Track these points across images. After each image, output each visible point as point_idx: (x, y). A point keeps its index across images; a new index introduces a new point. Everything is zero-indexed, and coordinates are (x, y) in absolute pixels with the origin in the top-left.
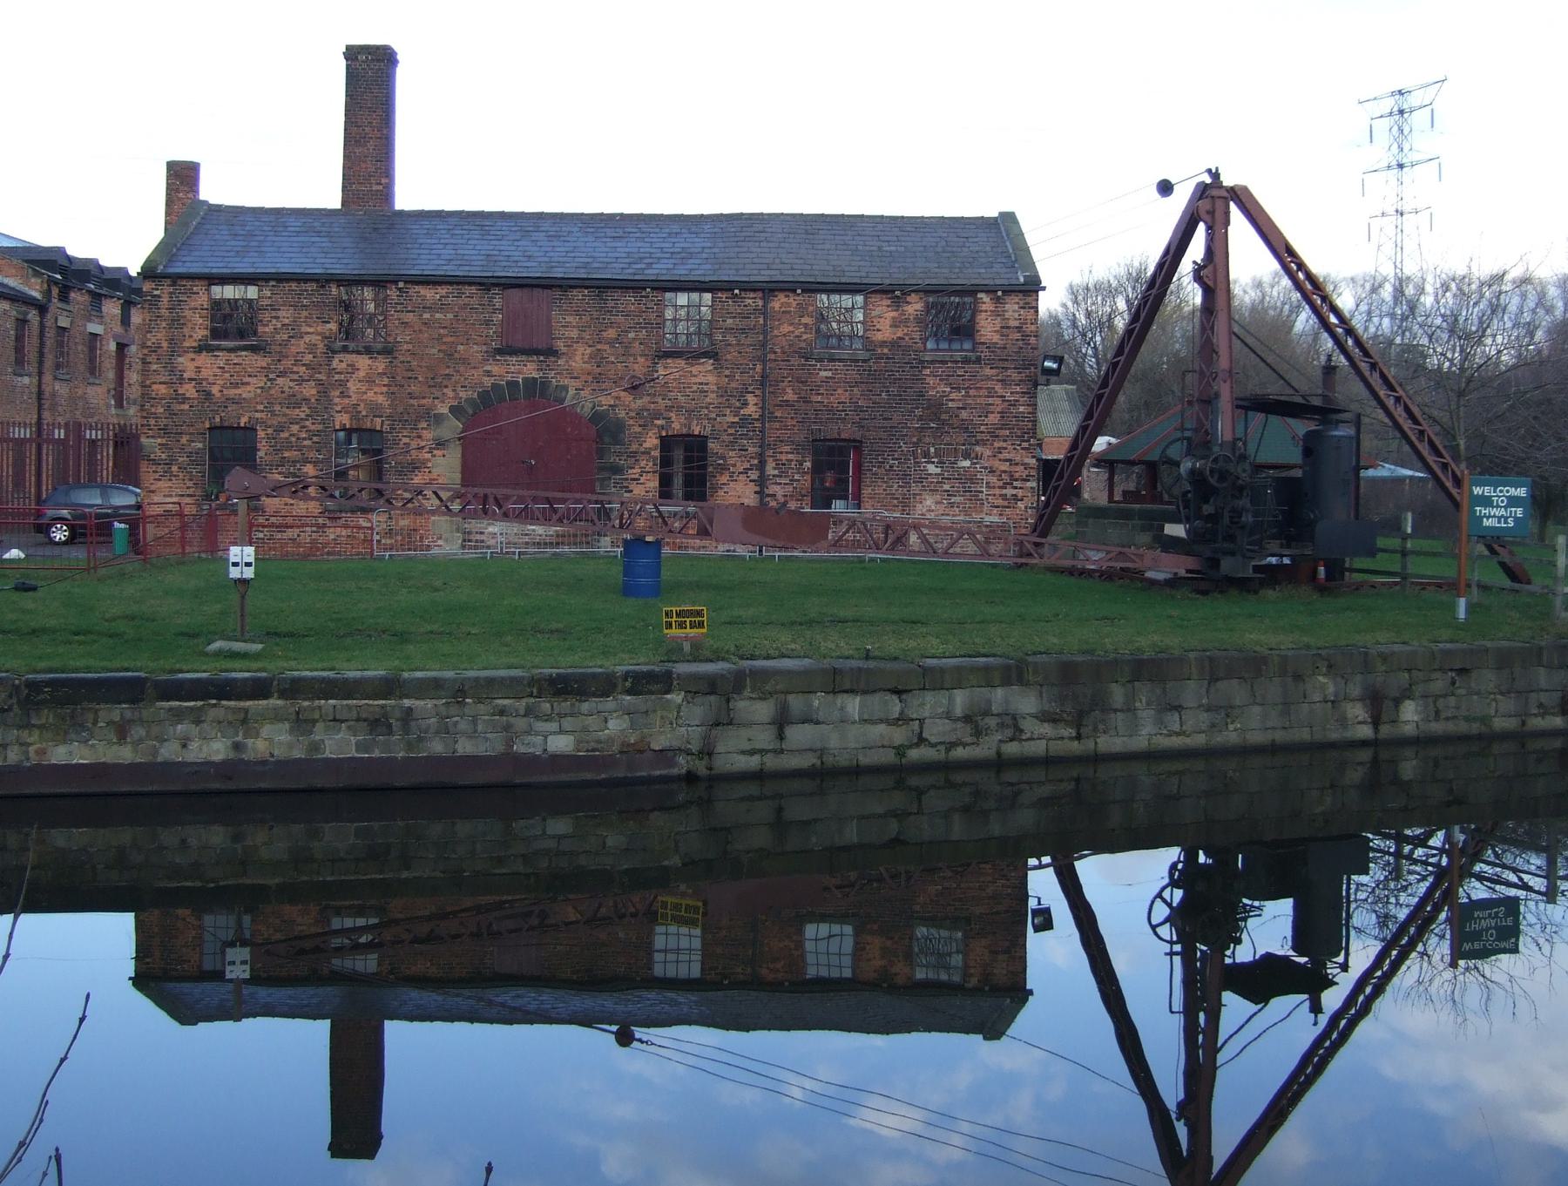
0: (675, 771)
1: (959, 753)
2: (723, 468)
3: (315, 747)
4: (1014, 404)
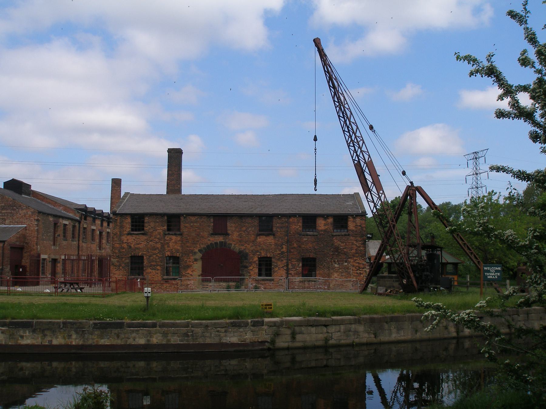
0: (265, 347)
1: (343, 342)
2: (276, 266)
3: (169, 340)
4: (360, 247)
